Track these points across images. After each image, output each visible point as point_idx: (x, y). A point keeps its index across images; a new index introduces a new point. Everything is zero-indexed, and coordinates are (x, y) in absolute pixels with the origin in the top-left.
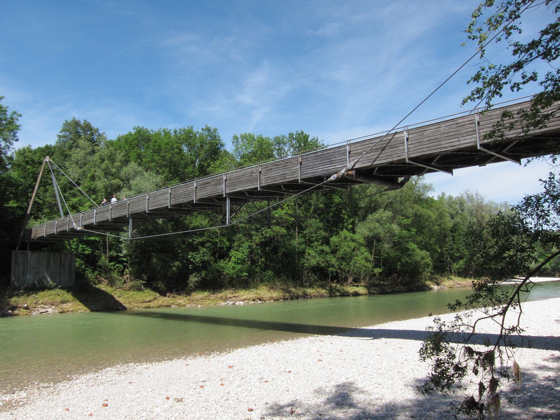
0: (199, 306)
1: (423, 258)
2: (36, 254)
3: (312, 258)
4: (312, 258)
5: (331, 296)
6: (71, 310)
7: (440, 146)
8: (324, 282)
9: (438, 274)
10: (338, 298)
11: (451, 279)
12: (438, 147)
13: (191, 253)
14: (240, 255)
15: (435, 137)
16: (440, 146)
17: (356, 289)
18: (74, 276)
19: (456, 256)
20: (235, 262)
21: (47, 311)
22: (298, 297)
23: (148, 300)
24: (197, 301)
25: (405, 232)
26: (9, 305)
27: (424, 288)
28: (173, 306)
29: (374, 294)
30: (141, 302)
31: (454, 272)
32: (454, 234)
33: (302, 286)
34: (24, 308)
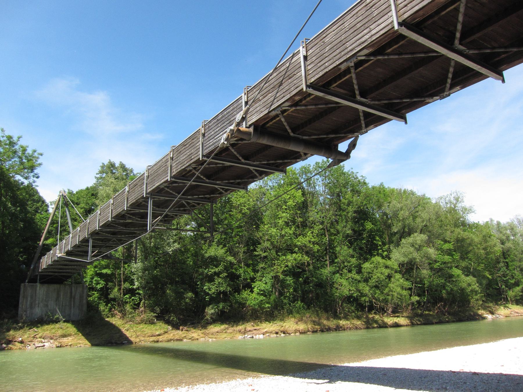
0: (210, 340)
1: (469, 285)
2: (45, 288)
3: (344, 286)
4: (344, 286)
5: (367, 328)
6: (70, 344)
7: (346, 51)
8: (360, 313)
9: (492, 302)
10: (376, 330)
11: (508, 307)
12: (343, 53)
13: (207, 284)
14: (263, 286)
15: (339, 40)
16: (346, 51)
17: (396, 320)
18: (85, 308)
19: (512, 284)
20: (258, 294)
21: (44, 346)
22: (329, 330)
23: (157, 333)
24: (212, 334)
25: (447, 258)
26: (5, 338)
27: (475, 318)
28: (185, 340)
29: (418, 324)
30: (149, 336)
31: (511, 300)
32: (507, 260)
33: (336, 316)
34: (19, 342)
